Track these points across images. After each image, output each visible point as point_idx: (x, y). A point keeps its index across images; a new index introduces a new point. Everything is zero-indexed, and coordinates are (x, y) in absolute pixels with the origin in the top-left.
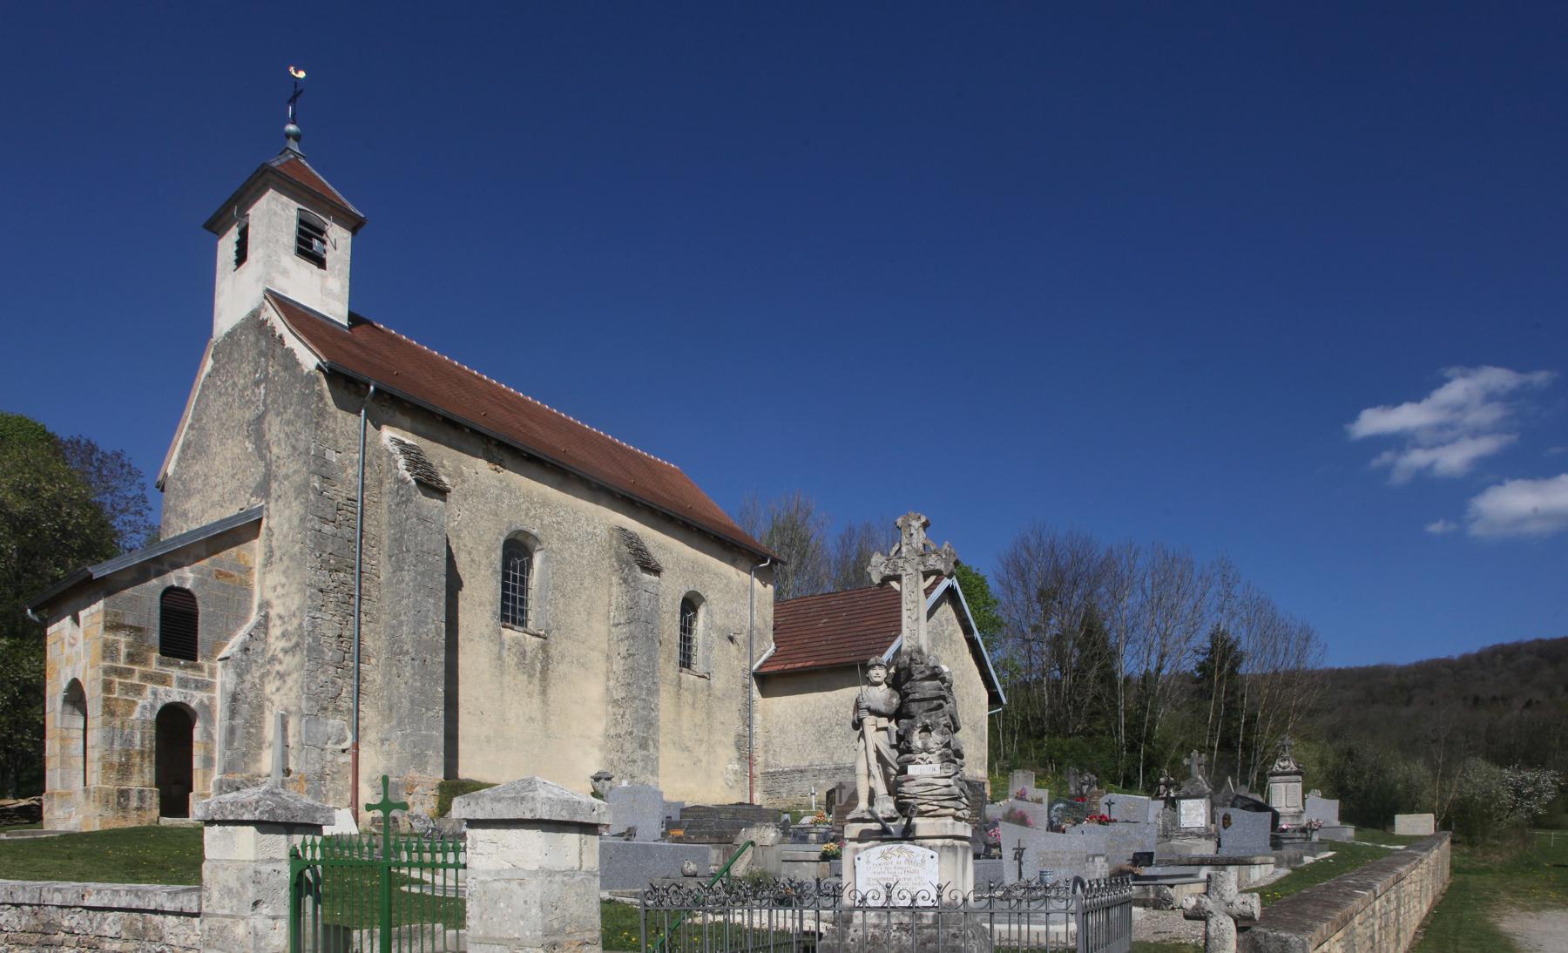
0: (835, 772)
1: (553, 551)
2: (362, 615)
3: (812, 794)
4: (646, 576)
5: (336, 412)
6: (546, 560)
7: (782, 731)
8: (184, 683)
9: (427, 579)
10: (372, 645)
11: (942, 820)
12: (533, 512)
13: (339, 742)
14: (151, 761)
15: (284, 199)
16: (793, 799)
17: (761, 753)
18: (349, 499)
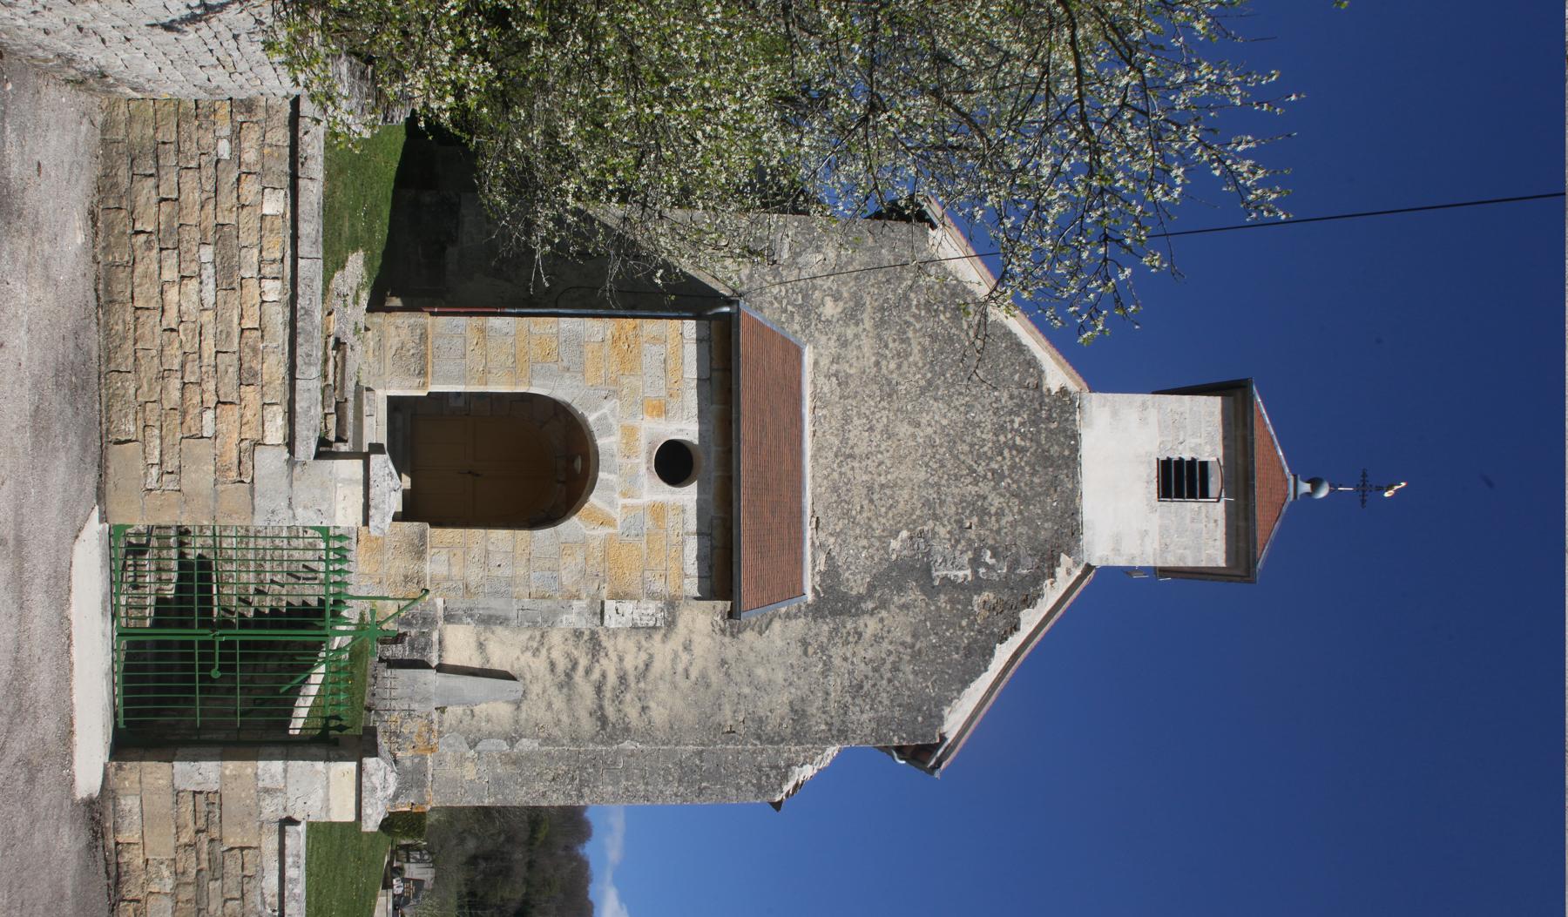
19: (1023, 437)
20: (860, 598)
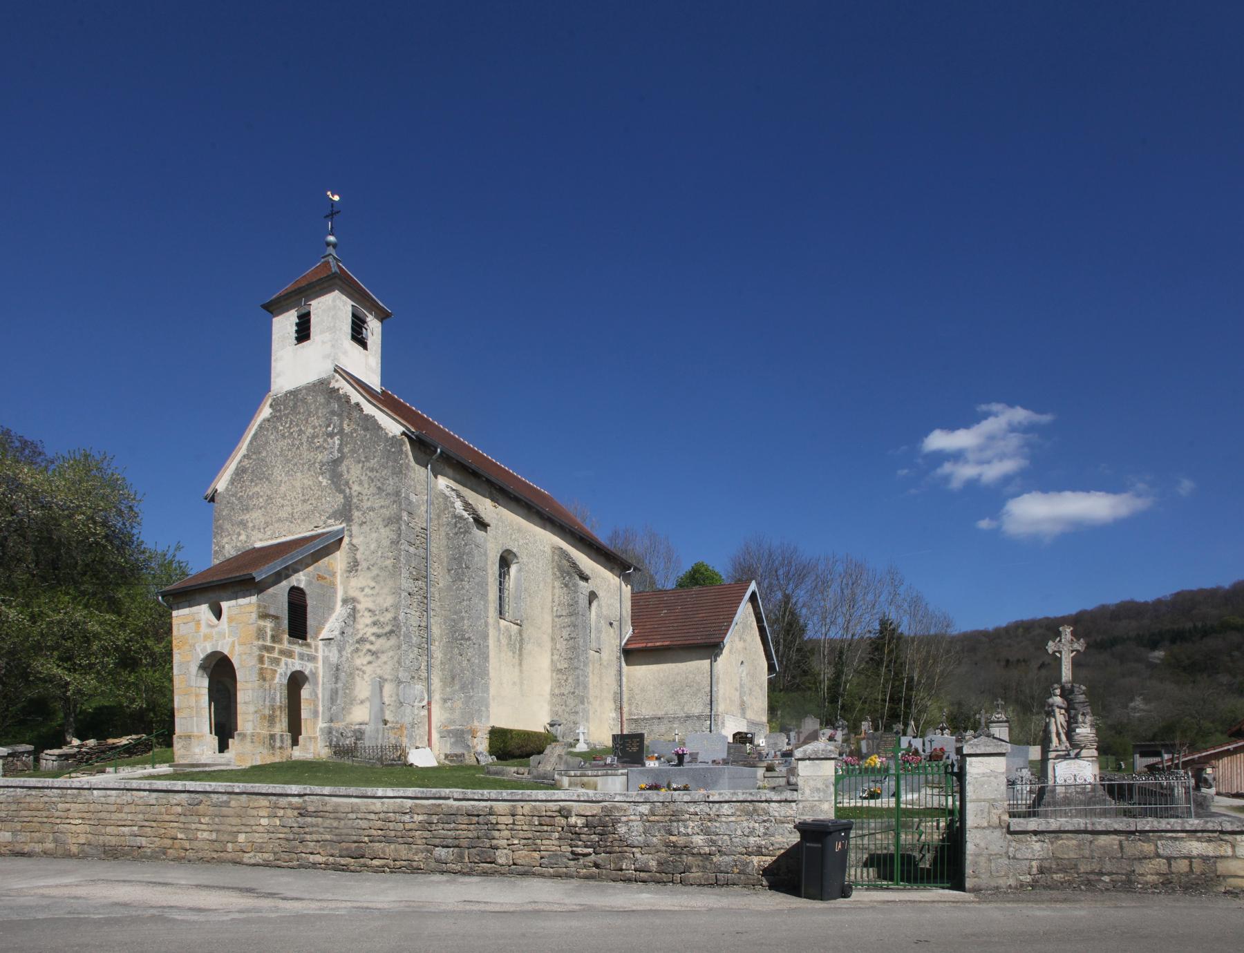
6: (520, 570)
7: (643, 690)
8: (302, 657)
11: (1091, 750)
13: (420, 701)
15: (344, 297)
19: (286, 423)
20: (345, 497)
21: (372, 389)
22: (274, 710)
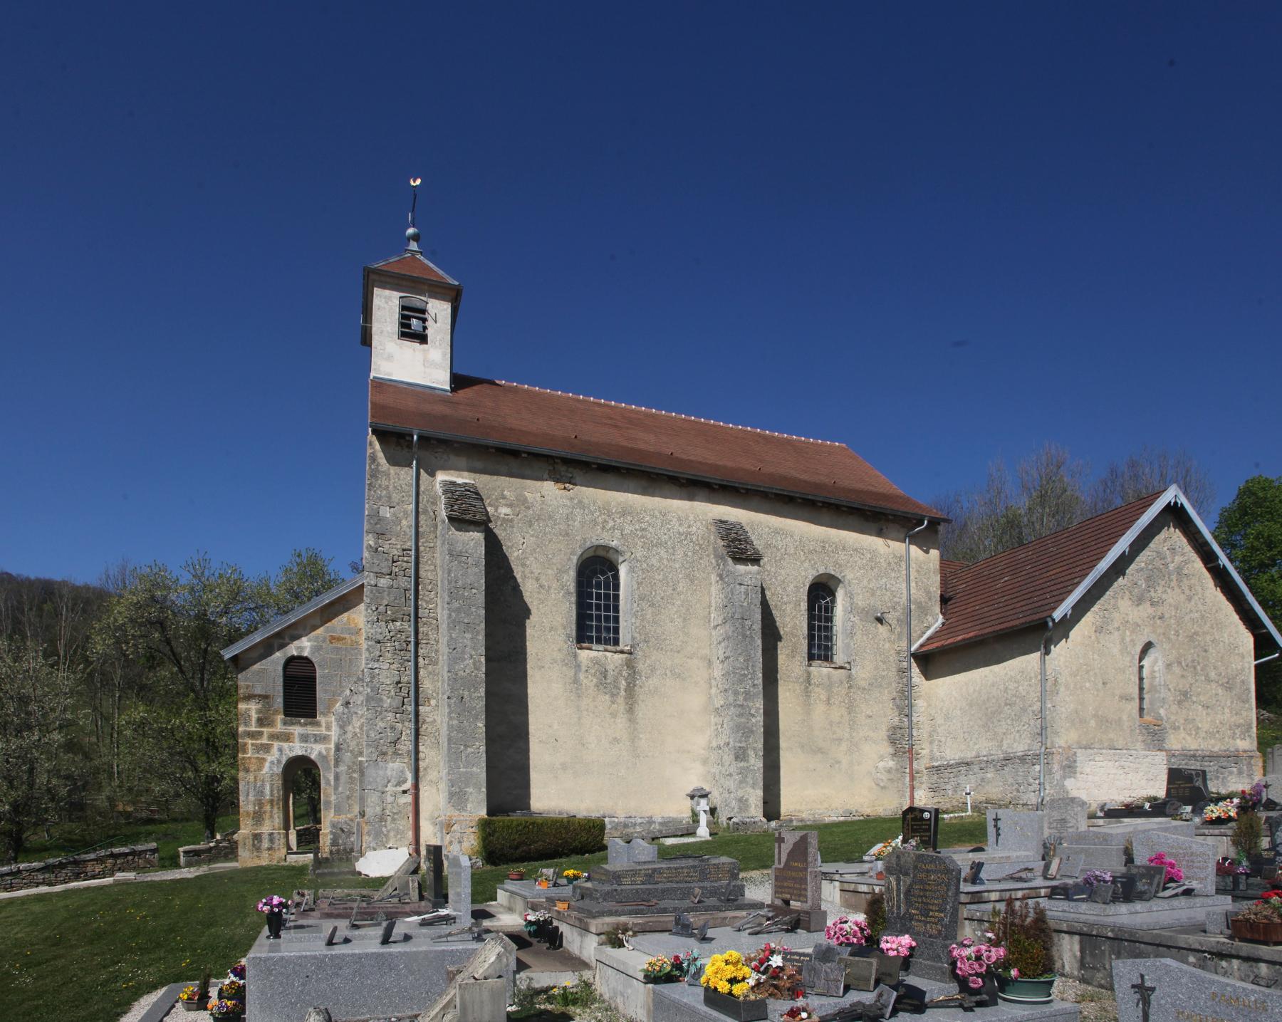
0: (1004, 763)
1: (638, 561)
2: (420, 659)
3: (966, 794)
4: (741, 568)
5: (389, 469)
6: (632, 570)
8: (305, 739)
9: (463, 615)
10: (431, 687)
12: (611, 524)
13: (399, 784)
14: (279, 808)
16: (959, 796)
17: (926, 745)
18: (404, 550)
21: (435, 388)
22: (261, 804)
